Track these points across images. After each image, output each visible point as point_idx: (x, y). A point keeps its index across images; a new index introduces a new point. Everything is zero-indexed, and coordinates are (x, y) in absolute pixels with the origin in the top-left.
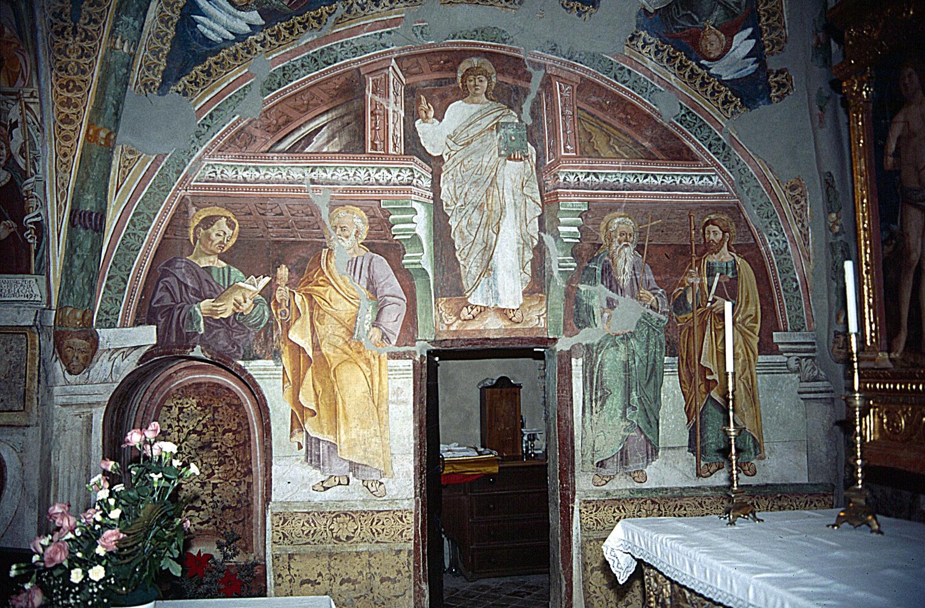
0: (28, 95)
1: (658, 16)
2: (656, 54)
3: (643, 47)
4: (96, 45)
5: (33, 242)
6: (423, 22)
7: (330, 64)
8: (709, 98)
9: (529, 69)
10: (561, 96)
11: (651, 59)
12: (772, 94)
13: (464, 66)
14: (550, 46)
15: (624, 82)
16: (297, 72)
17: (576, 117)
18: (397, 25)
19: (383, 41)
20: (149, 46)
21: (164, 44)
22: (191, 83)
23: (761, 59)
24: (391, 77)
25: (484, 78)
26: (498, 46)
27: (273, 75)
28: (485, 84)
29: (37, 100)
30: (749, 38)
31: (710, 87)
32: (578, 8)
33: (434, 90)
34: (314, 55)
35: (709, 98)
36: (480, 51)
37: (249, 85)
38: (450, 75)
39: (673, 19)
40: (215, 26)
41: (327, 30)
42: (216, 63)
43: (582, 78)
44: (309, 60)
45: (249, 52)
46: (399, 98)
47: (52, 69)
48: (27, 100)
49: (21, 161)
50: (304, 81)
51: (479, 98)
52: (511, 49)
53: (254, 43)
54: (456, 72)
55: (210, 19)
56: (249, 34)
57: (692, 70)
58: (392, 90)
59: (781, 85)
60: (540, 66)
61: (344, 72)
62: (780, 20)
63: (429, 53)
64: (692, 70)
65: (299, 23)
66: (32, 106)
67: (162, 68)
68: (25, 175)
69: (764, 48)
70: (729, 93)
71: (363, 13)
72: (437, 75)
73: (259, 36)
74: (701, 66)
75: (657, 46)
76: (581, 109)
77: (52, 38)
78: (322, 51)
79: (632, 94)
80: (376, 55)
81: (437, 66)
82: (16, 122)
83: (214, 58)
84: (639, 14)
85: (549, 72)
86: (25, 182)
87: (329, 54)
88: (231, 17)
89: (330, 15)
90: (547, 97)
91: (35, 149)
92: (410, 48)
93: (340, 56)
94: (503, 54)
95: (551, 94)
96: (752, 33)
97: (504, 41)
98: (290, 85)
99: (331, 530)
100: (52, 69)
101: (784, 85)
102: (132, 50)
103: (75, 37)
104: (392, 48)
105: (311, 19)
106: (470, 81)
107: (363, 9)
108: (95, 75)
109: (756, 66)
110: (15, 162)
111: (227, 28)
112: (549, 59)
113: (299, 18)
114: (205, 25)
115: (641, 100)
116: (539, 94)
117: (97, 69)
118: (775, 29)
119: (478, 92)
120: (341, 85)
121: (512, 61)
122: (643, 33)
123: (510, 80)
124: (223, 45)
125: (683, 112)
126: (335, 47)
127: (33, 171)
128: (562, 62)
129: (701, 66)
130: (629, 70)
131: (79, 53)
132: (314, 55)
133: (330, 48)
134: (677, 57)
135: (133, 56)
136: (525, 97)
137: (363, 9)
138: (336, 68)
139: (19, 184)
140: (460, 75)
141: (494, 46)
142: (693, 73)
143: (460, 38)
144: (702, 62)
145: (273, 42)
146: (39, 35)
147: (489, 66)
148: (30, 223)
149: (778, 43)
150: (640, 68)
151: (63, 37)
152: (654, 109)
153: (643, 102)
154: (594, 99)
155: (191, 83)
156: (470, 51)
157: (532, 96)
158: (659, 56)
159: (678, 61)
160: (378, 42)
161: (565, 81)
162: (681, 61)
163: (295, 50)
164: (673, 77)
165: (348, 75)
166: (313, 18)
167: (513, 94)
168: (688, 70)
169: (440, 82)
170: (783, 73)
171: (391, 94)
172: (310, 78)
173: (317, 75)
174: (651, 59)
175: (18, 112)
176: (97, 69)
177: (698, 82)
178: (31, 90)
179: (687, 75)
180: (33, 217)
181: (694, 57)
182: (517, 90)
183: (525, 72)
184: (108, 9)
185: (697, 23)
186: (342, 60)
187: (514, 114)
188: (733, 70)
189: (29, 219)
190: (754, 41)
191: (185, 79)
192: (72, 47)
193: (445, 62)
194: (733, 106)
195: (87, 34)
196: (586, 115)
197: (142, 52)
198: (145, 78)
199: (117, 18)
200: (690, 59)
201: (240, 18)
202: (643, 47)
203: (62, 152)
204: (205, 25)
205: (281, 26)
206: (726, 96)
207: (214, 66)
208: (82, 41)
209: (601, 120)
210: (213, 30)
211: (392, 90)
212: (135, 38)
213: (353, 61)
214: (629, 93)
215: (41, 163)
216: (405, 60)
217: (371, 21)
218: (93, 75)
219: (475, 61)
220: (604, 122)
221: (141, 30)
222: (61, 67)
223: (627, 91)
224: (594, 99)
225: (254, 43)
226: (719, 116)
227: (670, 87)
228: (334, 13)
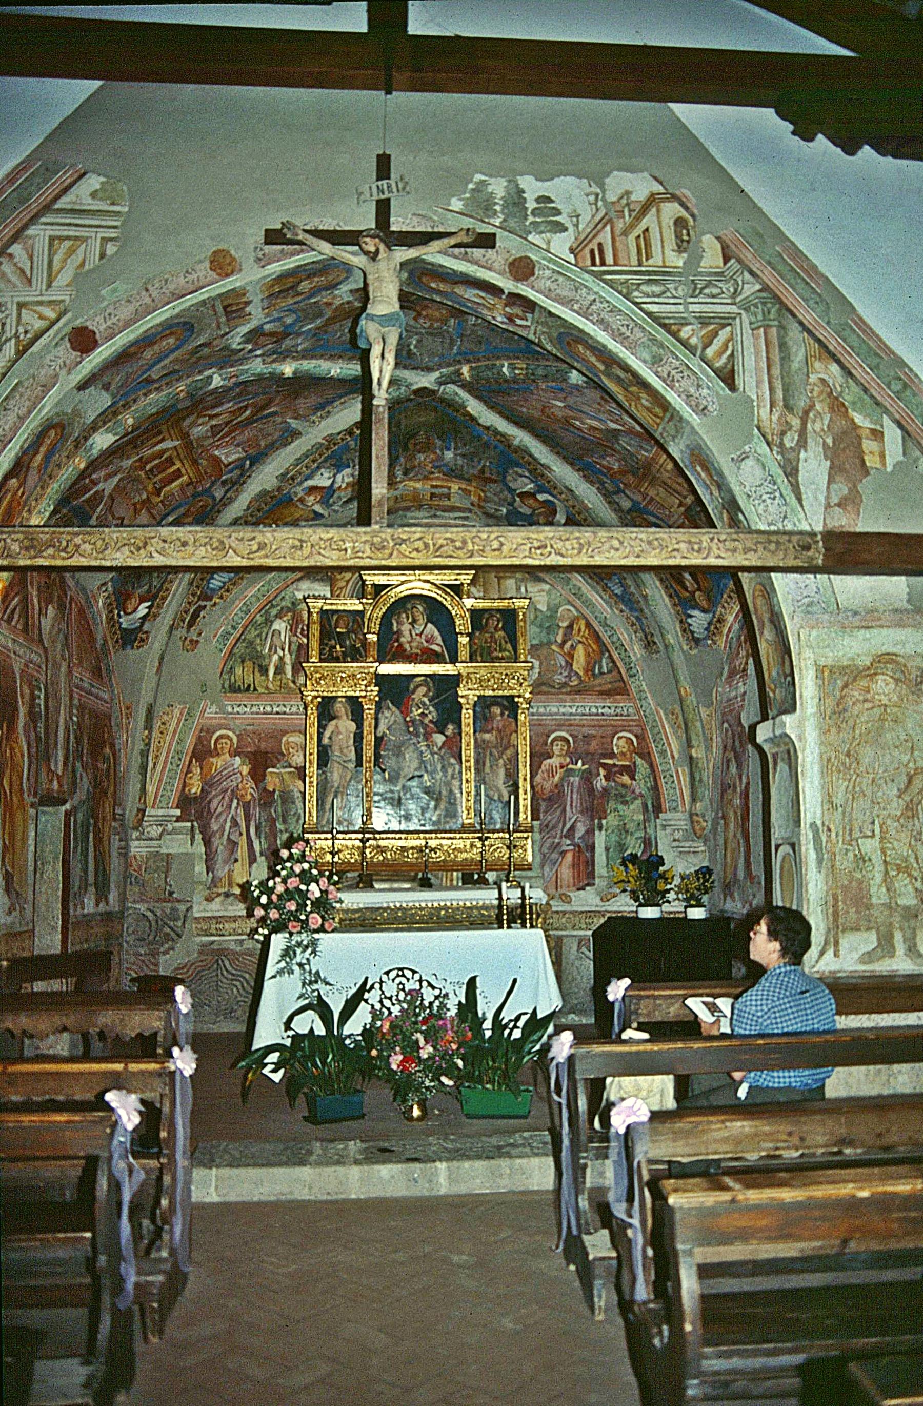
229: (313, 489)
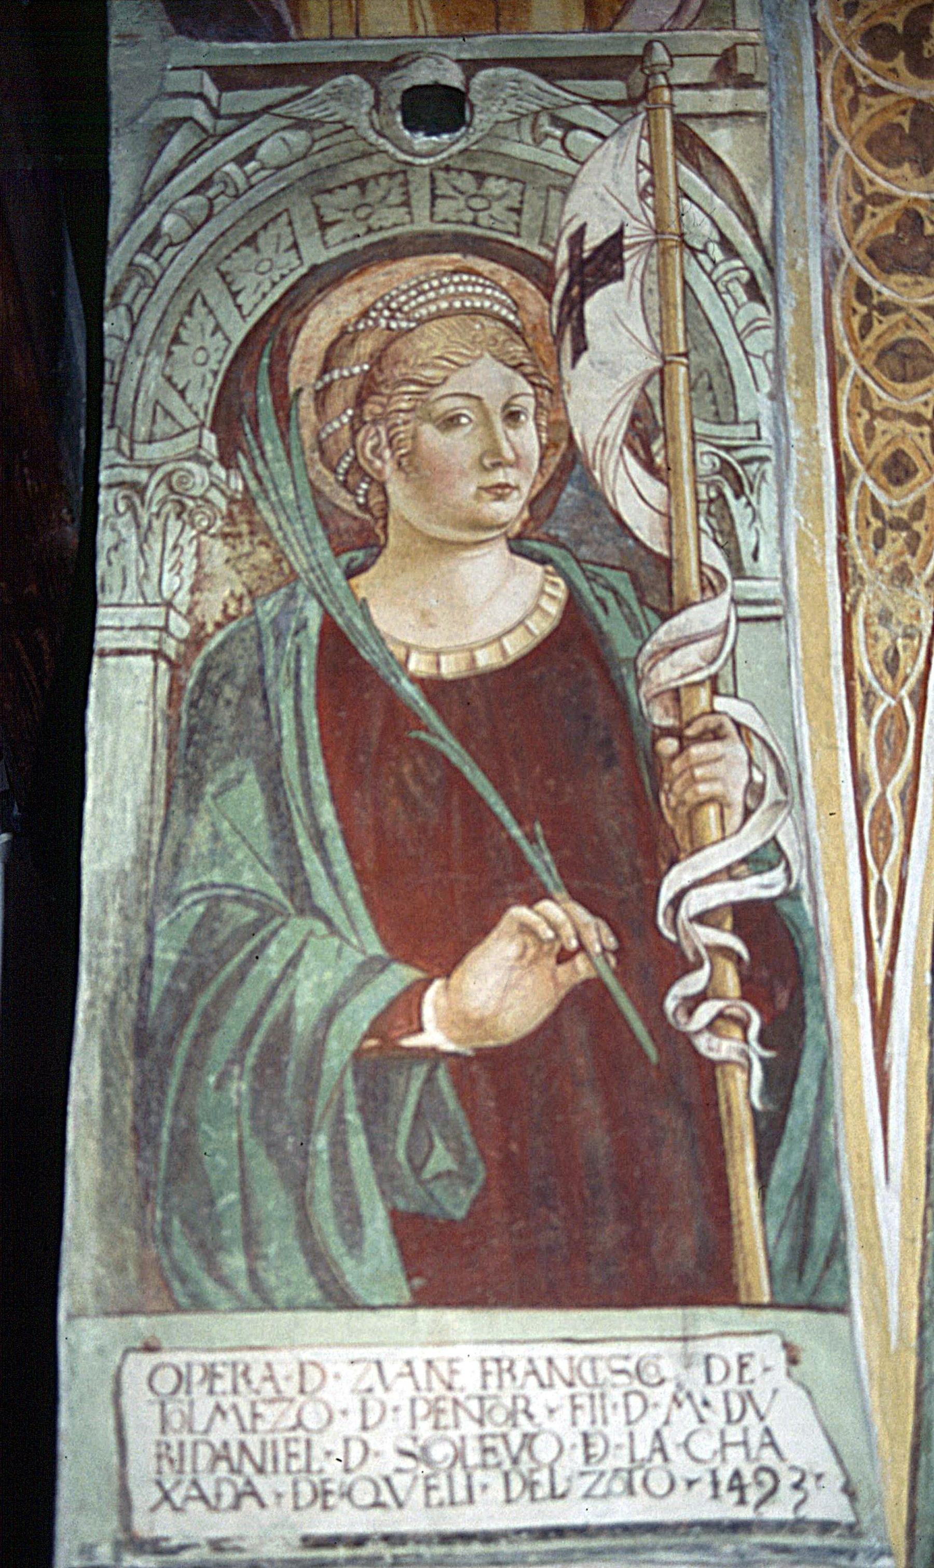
0: (703, 70)
5: (736, 1054)
29: (756, 99)
48: (688, 101)
49: (635, 498)
66: (722, 140)
68: (657, 585)
82: (614, 246)
86: (664, 633)
91: (724, 409)
99: (290, 1455)
110: (597, 504)
127: (715, 557)
139: (622, 641)
148: (701, 918)
175: (630, 179)
178: (724, 38)
180: (729, 873)
189: (700, 886)
203: (880, 450)
215: (767, 504)
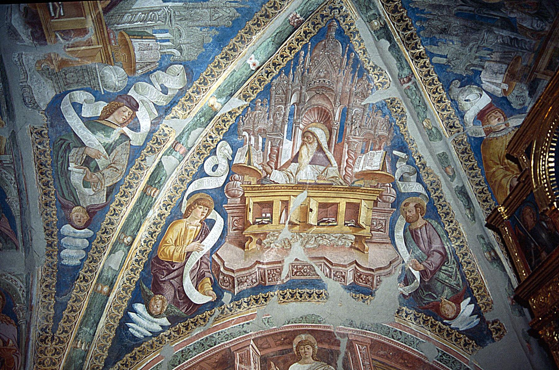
1: (411, 297)
2: (415, 320)
3: (406, 317)
4: (64, 347)
6: (268, 315)
7: (212, 346)
8: (454, 343)
9: (338, 338)
10: (360, 353)
11: (413, 323)
12: (494, 336)
13: (297, 340)
14: (349, 322)
15: (399, 340)
16: (190, 353)
17: (372, 365)
18: (252, 319)
19: (244, 329)
20: (98, 343)
21: (108, 342)
22: (123, 365)
23: (480, 315)
24: (251, 352)
25: (310, 347)
26: (316, 326)
27: (175, 356)
28: (311, 350)
30: (470, 304)
31: (453, 336)
32: (362, 298)
33: (279, 357)
34: (202, 342)
35: (454, 343)
36: (305, 330)
37: (160, 364)
38: (288, 347)
39: (421, 298)
40: (140, 329)
41: (209, 325)
42: (139, 351)
43: (372, 340)
44: (198, 345)
45: (161, 343)
46: (257, 365)
47: (35, 364)
50: (195, 359)
51: (308, 360)
52: (324, 326)
53: (164, 337)
54: (292, 345)
55: (137, 325)
56: (161, 332)
57: (439, 327)
58: (252, 360)
59: (498, 330)
60: (344, 336)
61: (220, 351)
62: (485, 291)
63: (273, 334)
64: (439, 327)
65: (192, 322)
67: (105, 357)
69: (480, 308)
70: (467, 338)
71: (231, 313)
72: (280, 348)
73: (167, 333)
74: (445, 324)
75: (414, 315)
76: (375, 360)
77: (38, 344)
78: (207, 338)
79: (405, 347)
80: (241, 338)
81: (279, 342)
83: (138, 348)
84: (400, 297)
85: (350, 338)
87: (211, 340)
88: (150, 322)
89: (211, 316)
90: (351, 354)
92: (262, 332)
93: (218, 341)
94: (320, 330)
95: (354, 352)
96: (471, 300)
97: (320, 322)
98: (186, 362)
100: (35, 364)
101: (500, 330)
102: (87, 348)
103: (52, 342)
104: (250, 333)
105: (199, 319)
106: (302, 349)
107: (231, 311)
108: (62, 365)
109: (479, 319)
111: (147, 329)
112: (349, 330)
113: (192, 320)
114: (133, 328)
115: (412, 350)
116: (346, 353)
117: (63, 361)
118: (484, 296)
119: (307, 356)
120: (219, 360)
121: (326, 334)
122: (404, 308)
123: (326, 346)
124: (143, 340)
125: (440, 354)
126: (214, 336)
128: (357, 331)
129: (445, 324)
130: (400, 332)
131: (53, 352)
132: (202, 342)
133: (212, 336)
134: (429, 320)
135: (87, 351)
136: (338, 356)
137: (231, 311)
138: (215, 348)
140: (294, 346)
141: (314, 326)
142: (441, 329)
143: (292, 323)
144: (444, 321)
145: (176, 335)
146: (31, 342)
147: (312, 339)
149: (488, 305)
150: (407, 329)
151: (45, 343)
152: (421, 355)
153: (413, 351)
154: (382, 353)
155: (123, 365)
156: (299, 330)
157: (342, 355)
158: (418, 321)
159: (430, 323)
160: (242, 330)
161: (361, 343)
162: (431, 322)
163: (189, 339)
164: (429, 333)
165: (223, 353)
166: (201, 319)
167: (330, 355)
168: (437, 327)
169: (282, 352)
170: (497, 322)
171: (252, 363)
172: (199, 356)
173: (204, 354)
174: (413, 323)
176: (63, 361)
177: (445, 334)
179: (437, 330)
181: (439, 318)
182: (332, 352)
183: (336, 340)
184: (75, 323)
185: (436, 298)
186: (219, 343)
187: (332, 368)
188: (465, 323)
190: (473, 305)
191: (119, 363)
192: (49, 349)
193: (285, 339)
194: (471, 346)
195: (60, 340)
196: (379, 363)
197: (93, 348)
198: (93, 365)
199: (81, 329)
200: (437, 320)
201: (156, 322)
202: (406, 317)
204: (133, 328)
205: (180, 325)
206: (465, 340)
207: (138, 353)
208: (56, 344)
209: (388, 366)
210: (138, 331)
211: (252, 360)
212: (90, 340)
213: (226, 344)
214: (403, 346)
216: (259, 340)
217: (236, 317)
218: (60, 366)
219: (303, 336)
220: (391, 367)
221: (94, 335)
222: (40, 362)
223: (401, 345)
224: (382, 353)
225: (164, 337)
226: (464, 354)
227: (428, 339)
228: (213, 314)
229: (482, 116)
